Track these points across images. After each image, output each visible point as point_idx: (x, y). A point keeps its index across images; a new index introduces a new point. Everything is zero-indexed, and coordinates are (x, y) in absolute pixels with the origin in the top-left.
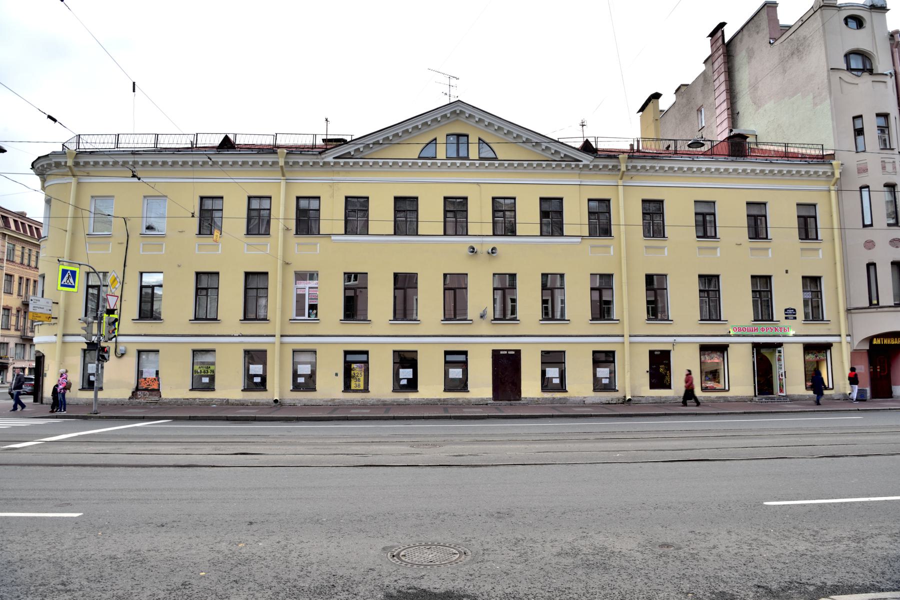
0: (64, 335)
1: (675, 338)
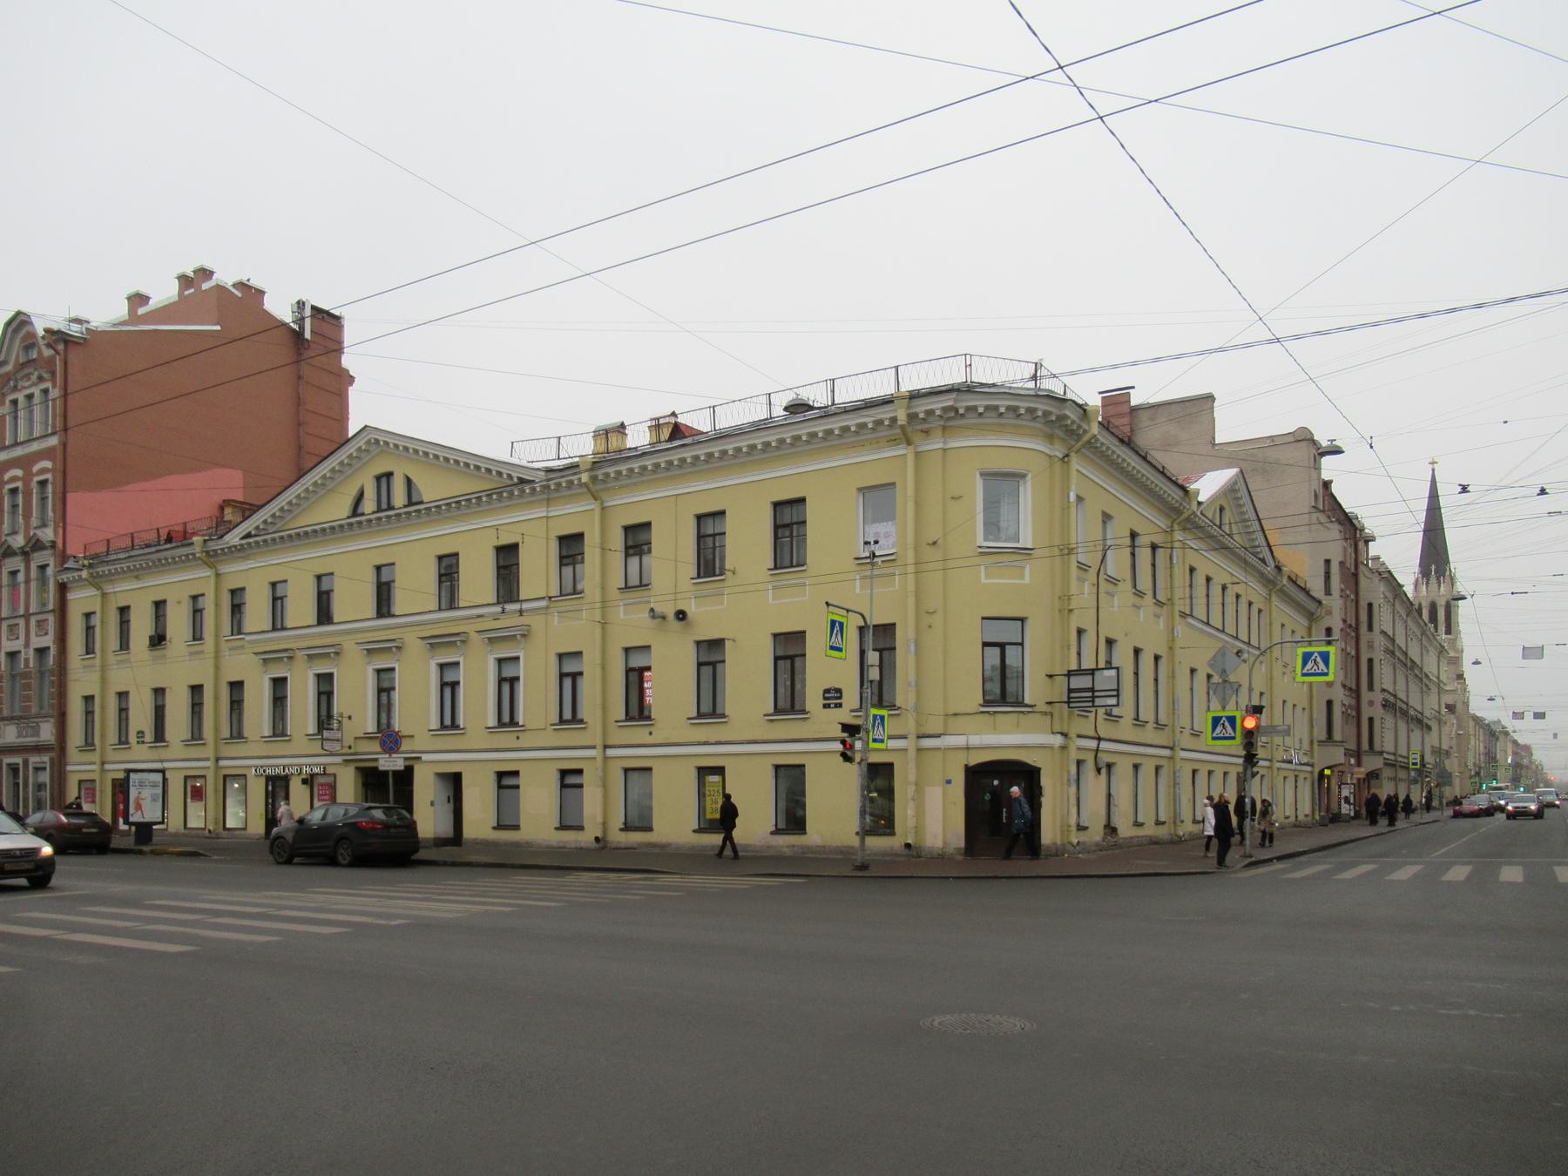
0: (606, 747)
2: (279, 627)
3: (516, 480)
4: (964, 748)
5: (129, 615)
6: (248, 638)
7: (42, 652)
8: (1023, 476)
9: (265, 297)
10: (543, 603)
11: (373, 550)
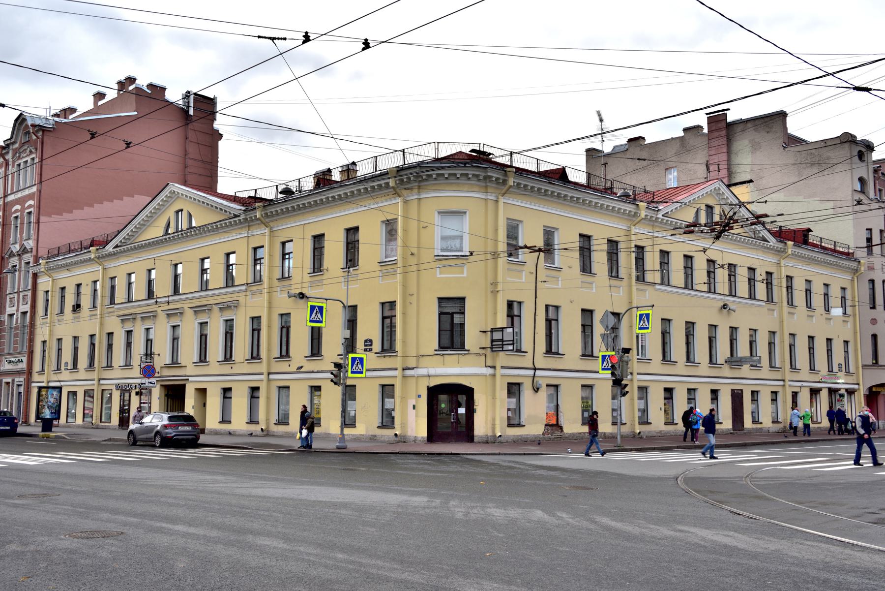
0: (269, 374)
1: (802, 383)
2: (230, 285)
3: (232, 215)
4: (426, 376)
5: (358, 236)
6: (116, 306)
7: (25, 313)
8: (465, 213)
9: (166, 92)
10: (244, 287)
11: (173, 255)
